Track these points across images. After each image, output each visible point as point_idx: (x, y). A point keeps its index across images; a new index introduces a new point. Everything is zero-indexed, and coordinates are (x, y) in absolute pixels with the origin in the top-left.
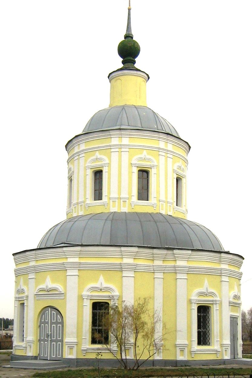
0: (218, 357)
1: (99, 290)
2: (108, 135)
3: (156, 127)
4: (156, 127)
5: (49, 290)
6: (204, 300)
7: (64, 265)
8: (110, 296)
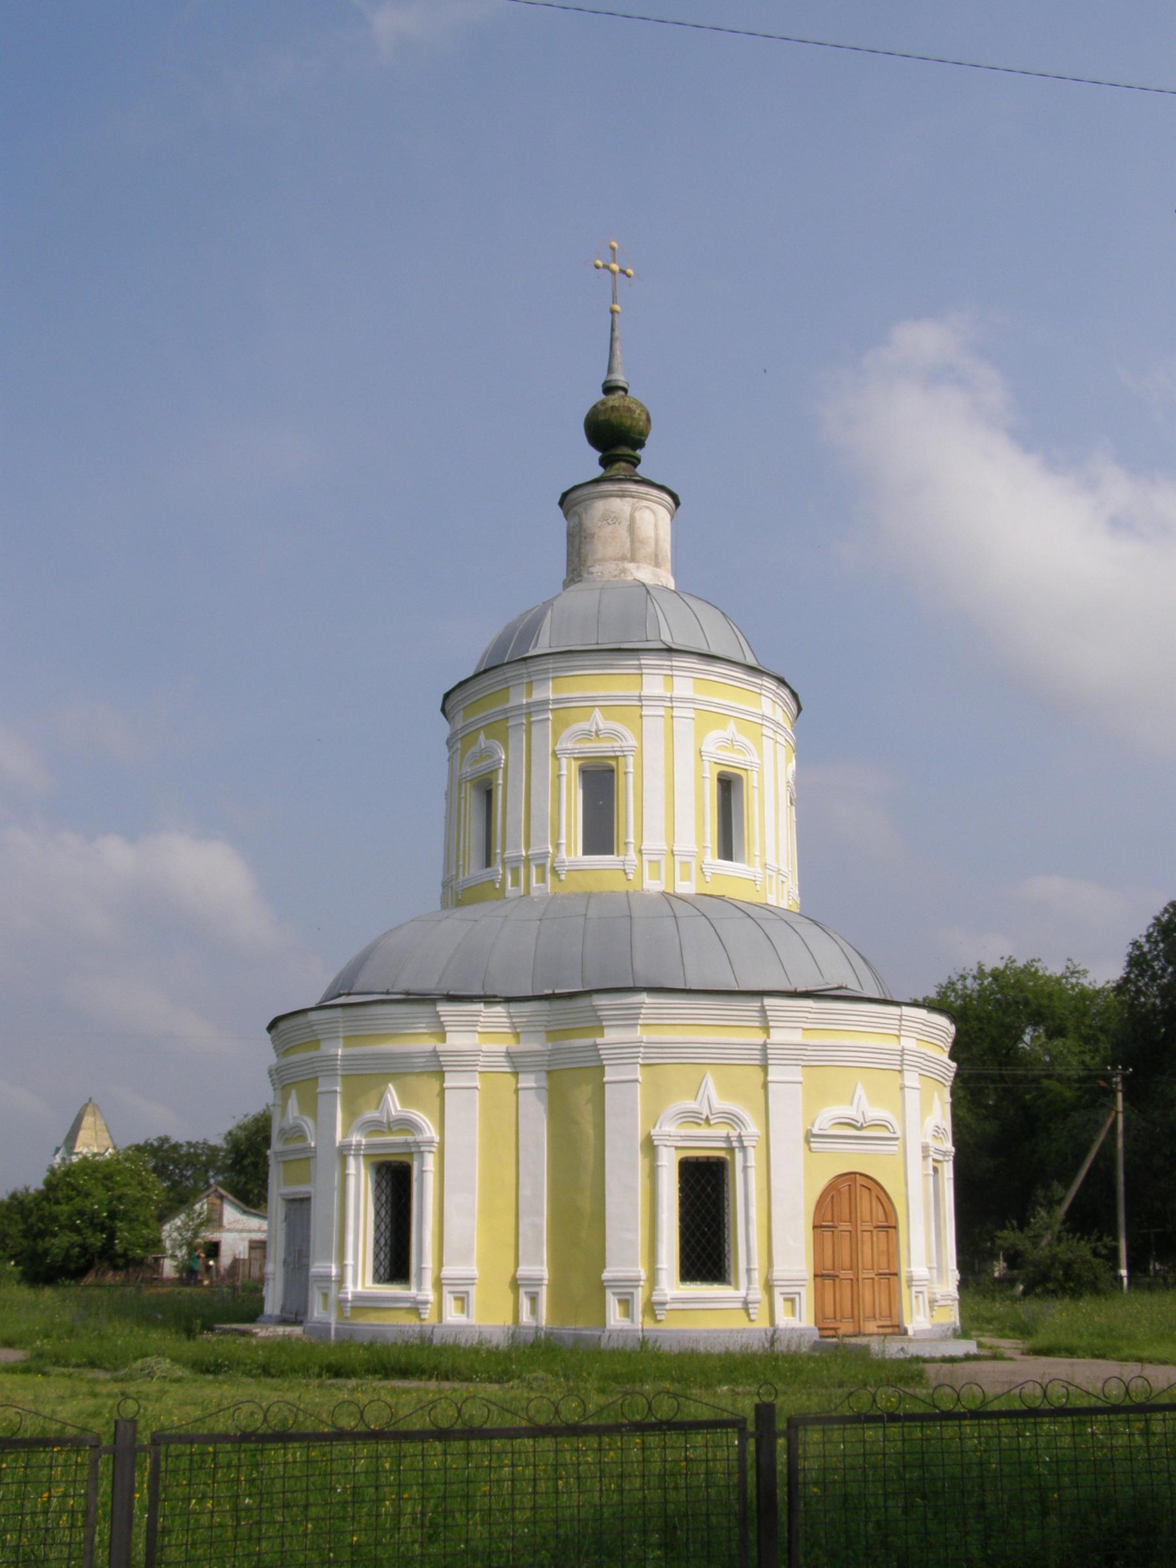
2: (755, 684)
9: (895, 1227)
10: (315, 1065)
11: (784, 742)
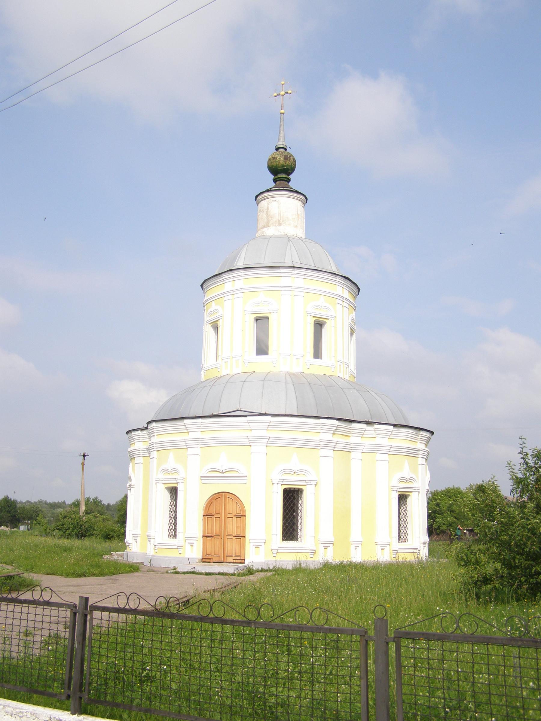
0: (156, 552)
1: (293, 473)
3: (329, 267)
4: (329, 267)
5: (224, 471)
6: (293, 482)
7: (185, 442)
8: (307, 481)
9: (245, 516)
10: (133, 453)
11: (347, 306)
